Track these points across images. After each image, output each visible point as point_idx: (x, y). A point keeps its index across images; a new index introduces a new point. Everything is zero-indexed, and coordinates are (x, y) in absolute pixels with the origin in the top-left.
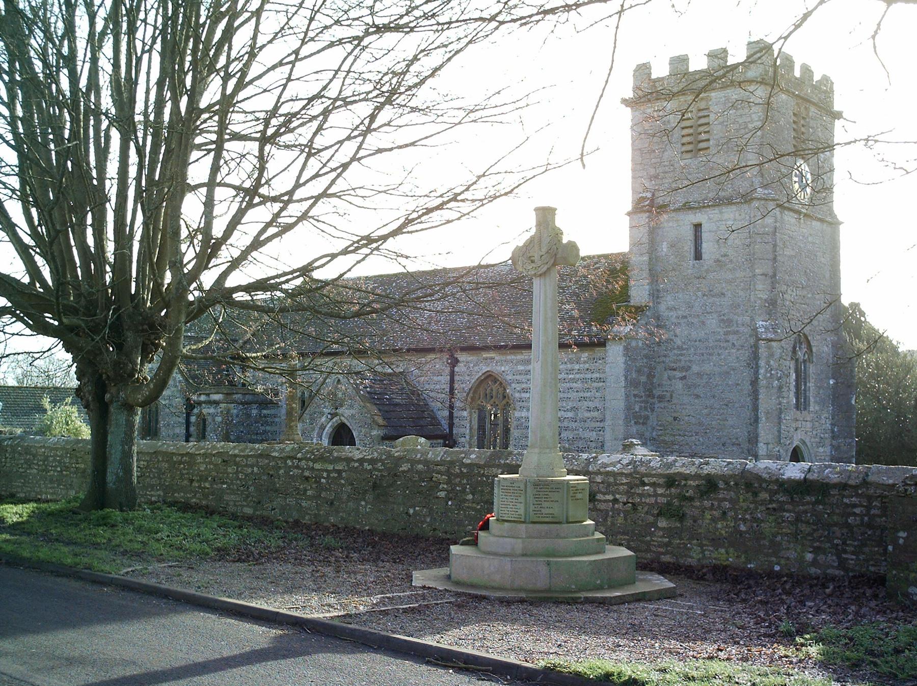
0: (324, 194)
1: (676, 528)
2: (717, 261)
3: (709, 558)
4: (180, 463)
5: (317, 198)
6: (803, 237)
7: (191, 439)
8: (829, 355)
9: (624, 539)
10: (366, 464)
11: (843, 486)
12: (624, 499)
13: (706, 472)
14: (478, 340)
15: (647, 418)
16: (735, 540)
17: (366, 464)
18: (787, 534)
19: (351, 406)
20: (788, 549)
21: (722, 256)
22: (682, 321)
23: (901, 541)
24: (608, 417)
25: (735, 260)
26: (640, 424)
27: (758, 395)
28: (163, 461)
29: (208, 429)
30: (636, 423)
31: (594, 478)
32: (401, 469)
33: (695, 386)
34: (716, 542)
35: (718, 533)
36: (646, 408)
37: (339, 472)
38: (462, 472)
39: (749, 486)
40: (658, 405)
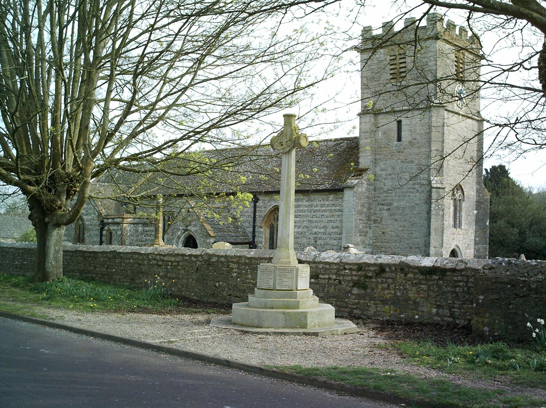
0: (174, 104)
1: (363, 294)
2: (411, 142)
3: (380, 311)
4: (89, 257)
5: (169, 108)
6: (461, 128)
7: (103, 244)
8: (474, 197)
9: (334, 301)
10: (193, 258)
11: (453, 270)
12: (334, 277)
13: (379, 262)
14: (271, 188)
15: (367, 232)
16: (395, 301)
17: (193, 258)
18: (422, 298)
19: (195, 226)
20: (423, 306)
21: (413, 139)
22: (389, 177)
23: (480, 301)
24: (344, 232)
25: (420, 142)
26: (362, 236)
27: (430, 219)
28: (80, 256)
29: (113, 238)
30: (360, 235)
31: (318, 266)
32: (212, 261)
33: (394, 214)
34: (384, 302)
35: (385, 297)
36: (366, 227)
37: (178, 262)
38: (245, 262)
39: (402, 270)
40: (374, 225)
